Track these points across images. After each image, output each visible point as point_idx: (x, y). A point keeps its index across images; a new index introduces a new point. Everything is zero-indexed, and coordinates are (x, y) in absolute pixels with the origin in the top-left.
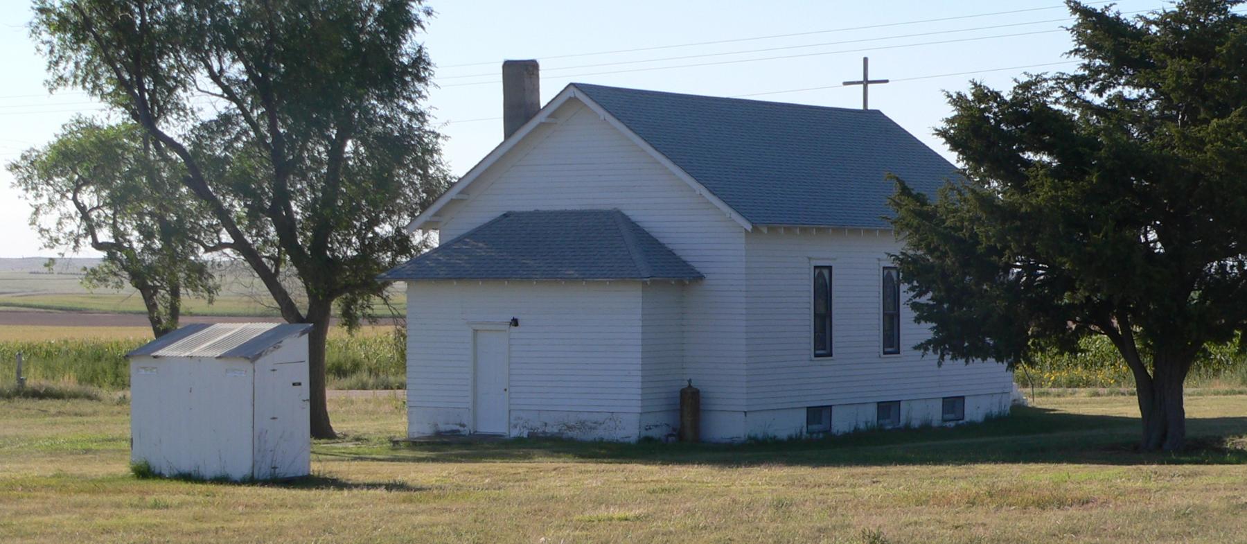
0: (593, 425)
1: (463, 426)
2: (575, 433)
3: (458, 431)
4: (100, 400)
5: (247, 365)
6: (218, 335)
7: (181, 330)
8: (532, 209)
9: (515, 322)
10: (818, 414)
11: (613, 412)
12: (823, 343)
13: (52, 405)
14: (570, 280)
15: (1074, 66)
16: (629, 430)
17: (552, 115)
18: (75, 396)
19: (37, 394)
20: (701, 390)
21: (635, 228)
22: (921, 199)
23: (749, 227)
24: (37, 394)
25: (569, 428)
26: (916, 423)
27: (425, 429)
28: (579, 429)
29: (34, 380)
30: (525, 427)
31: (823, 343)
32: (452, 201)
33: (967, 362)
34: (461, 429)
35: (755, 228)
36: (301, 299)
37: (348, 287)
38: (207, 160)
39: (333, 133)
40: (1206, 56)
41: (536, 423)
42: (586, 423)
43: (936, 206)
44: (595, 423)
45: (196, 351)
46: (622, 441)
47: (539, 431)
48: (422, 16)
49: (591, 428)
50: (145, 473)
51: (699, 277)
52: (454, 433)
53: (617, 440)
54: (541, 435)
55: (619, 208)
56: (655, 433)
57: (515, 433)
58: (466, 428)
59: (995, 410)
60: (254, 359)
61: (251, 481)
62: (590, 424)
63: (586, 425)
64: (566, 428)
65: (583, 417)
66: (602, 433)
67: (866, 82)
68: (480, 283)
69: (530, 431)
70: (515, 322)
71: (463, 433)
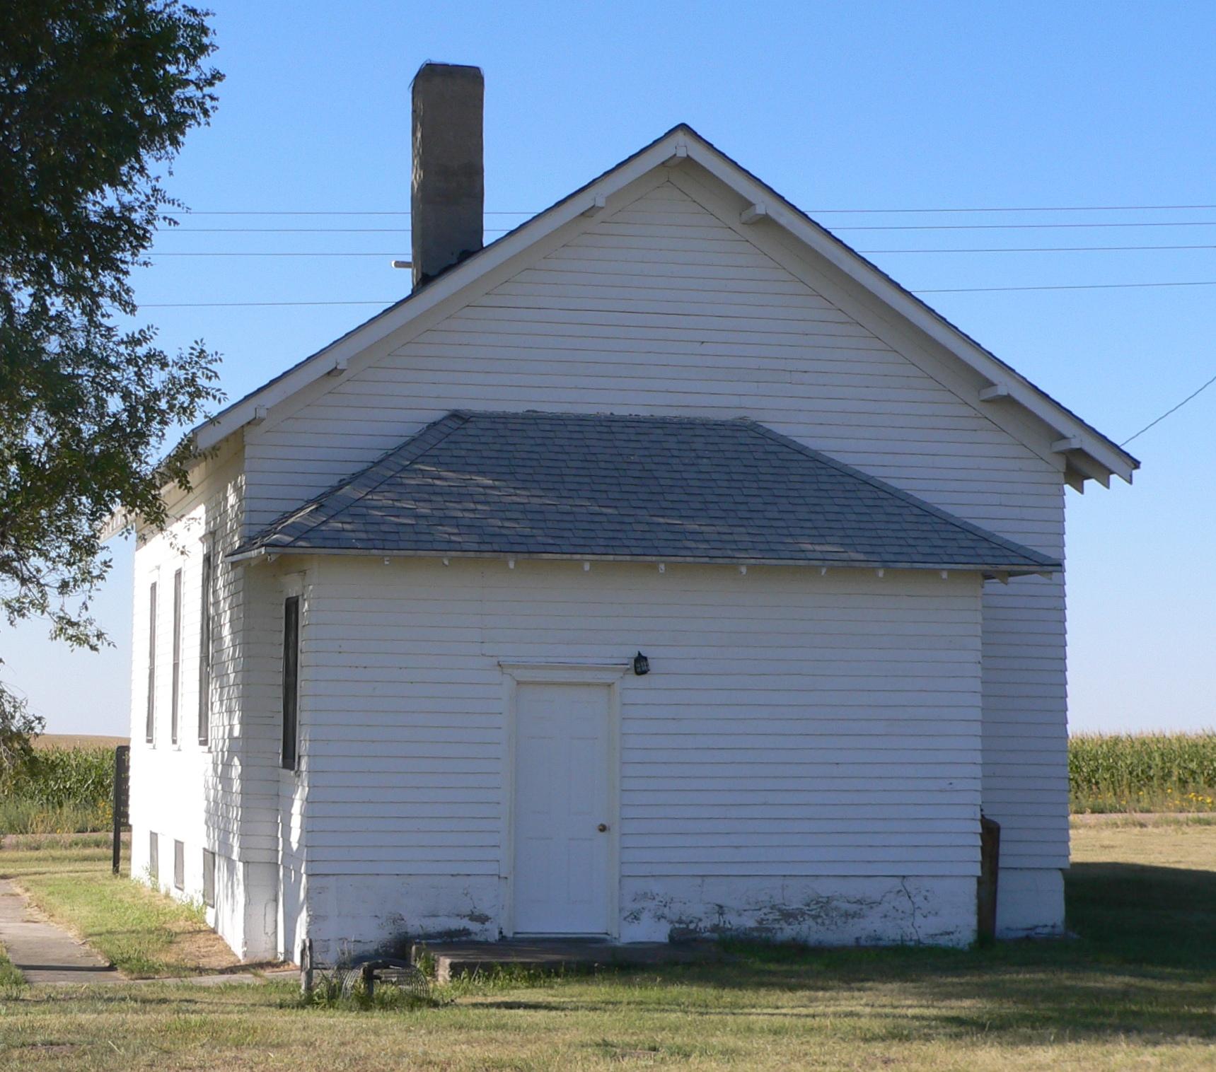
0: (855, 907)
1: (483, 919)
2: (805, 927)
3: (466, 932)
4: (893, 1061)
6: (311, 511)
7: (487, 247)
8: (521, 408)
9: (640, 665)
11: (904, 877)
20: (1002, 825)
25: (788, 916)
28: (815, 917)
30: (663, 917)
34: (474, 927)
39: (14, 73)
42: (835, 903)
44: (859, 902)
46: (930, 941)
47: (701, 925)
49: (847, 915)
53: (919, 941)
54: (707, 934)
55: (754, 416)
58: (488, 925)
62: (845, 906)
63: (836, 908)
64: (777, 915)
65: (825, 889)
66: (873, 926)
68: (512, 565)
69: (677, 925)
70: (640, 665)
71: (478, 938)
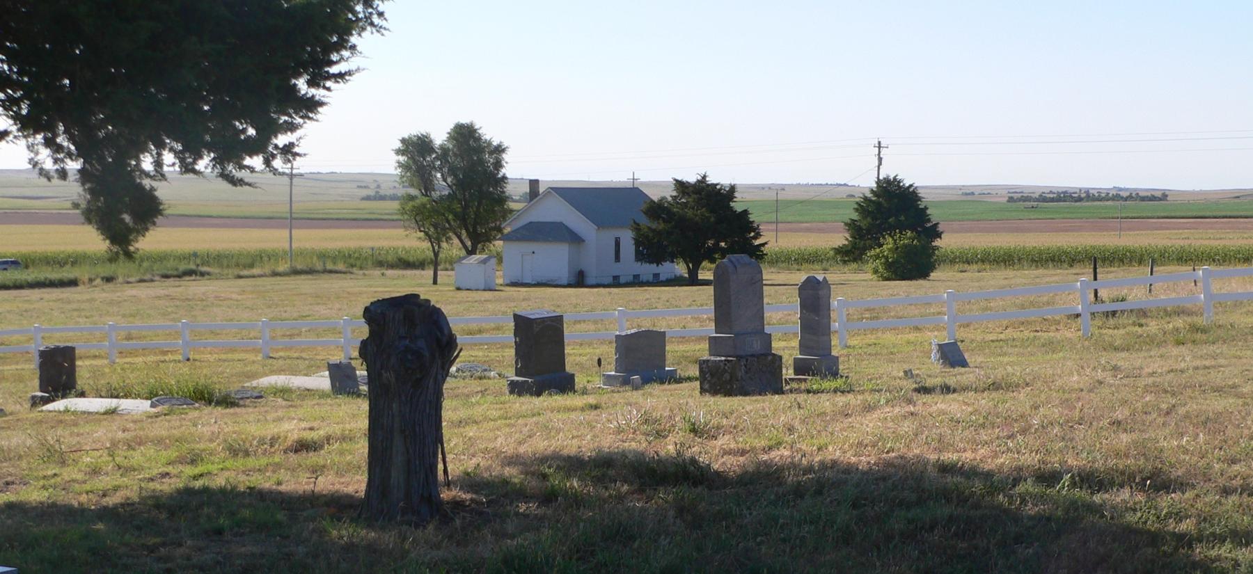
5: (483, 265)
9: (533, 253)
10: (616, 278)
12: (617, 258)
13: (333, 275)
14: (551, 241)
15: (675, 194)
16: (565, 282)
17: (544, 196)
18: (344, 273)
19: (331, 272)
21: (567, 228)
22: (638, 225)
23: (596, 228)
24: (331, 272)
26: (644, 281)
27: (508, 282)
29: (330, 266)
31: (617, 258)
32: (515, 219)
33: (658, 265)
35: (599, 228)
36: (469, 244)
37: (483, 241)
38: (1049, 509)
40: (701, 194)
41: (539, 280)
43: (239, 482)
45: (471, 262)
48: (505, 164)
50: (458, 289)
51: (583, 241)
52: (516, 282)
56: (571, 283)
57: (533, 282)
59: (669, 278)
60: (485, 264)
61: (484, 290)
67: (634, 179)
70: (533, 253)
